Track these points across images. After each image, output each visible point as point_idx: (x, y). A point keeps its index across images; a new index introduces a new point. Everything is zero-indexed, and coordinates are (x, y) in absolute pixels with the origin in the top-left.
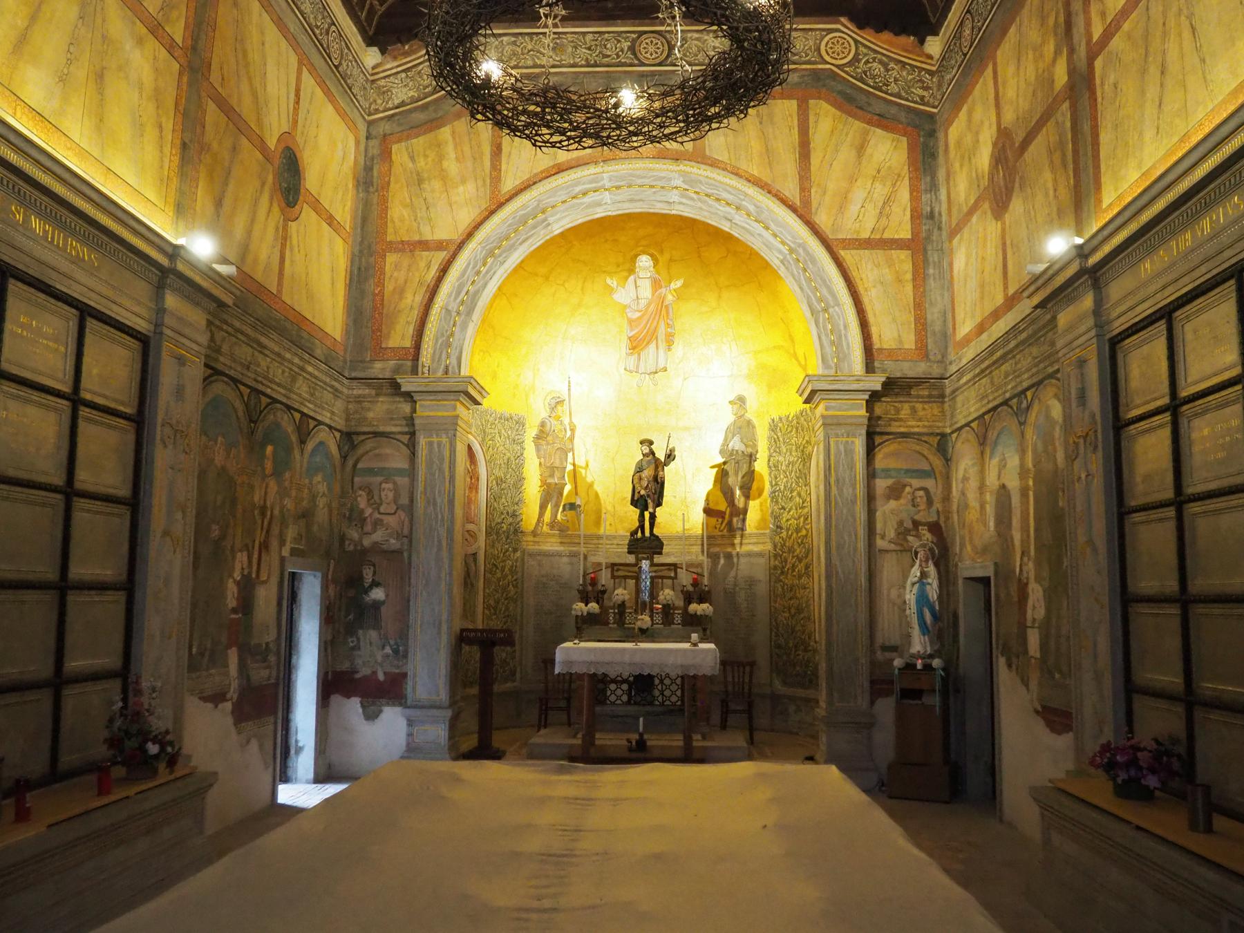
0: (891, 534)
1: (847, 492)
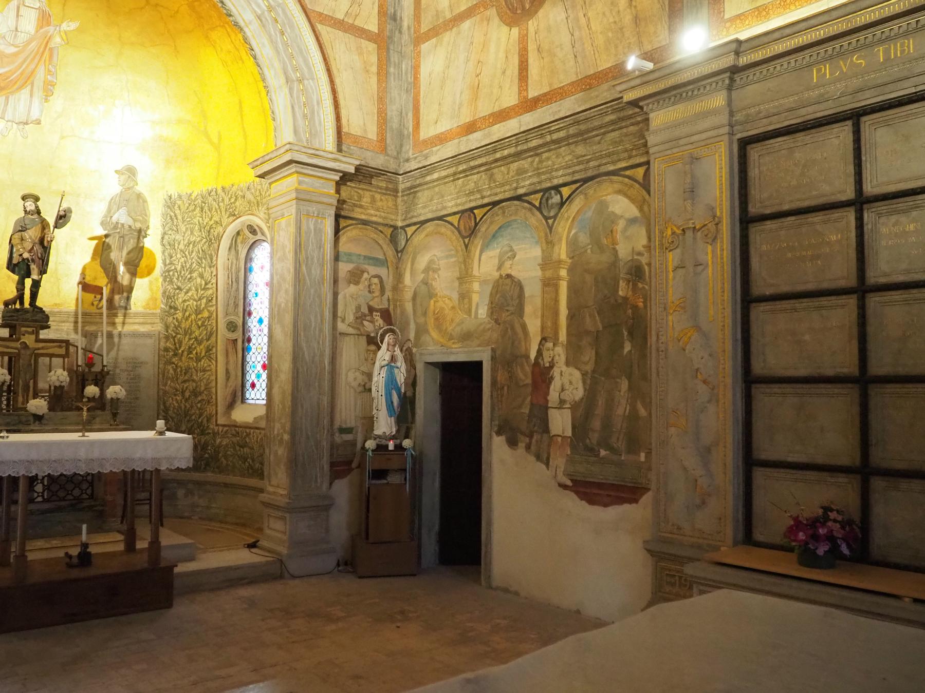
0: (351, 318)
1: (316, 272)
